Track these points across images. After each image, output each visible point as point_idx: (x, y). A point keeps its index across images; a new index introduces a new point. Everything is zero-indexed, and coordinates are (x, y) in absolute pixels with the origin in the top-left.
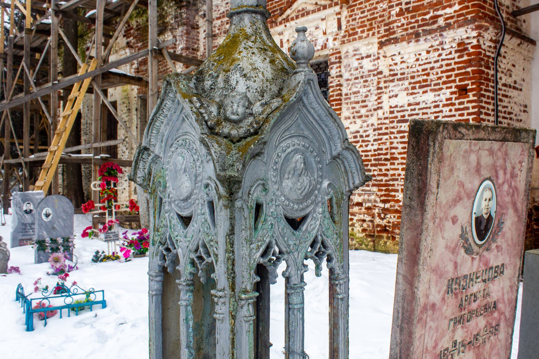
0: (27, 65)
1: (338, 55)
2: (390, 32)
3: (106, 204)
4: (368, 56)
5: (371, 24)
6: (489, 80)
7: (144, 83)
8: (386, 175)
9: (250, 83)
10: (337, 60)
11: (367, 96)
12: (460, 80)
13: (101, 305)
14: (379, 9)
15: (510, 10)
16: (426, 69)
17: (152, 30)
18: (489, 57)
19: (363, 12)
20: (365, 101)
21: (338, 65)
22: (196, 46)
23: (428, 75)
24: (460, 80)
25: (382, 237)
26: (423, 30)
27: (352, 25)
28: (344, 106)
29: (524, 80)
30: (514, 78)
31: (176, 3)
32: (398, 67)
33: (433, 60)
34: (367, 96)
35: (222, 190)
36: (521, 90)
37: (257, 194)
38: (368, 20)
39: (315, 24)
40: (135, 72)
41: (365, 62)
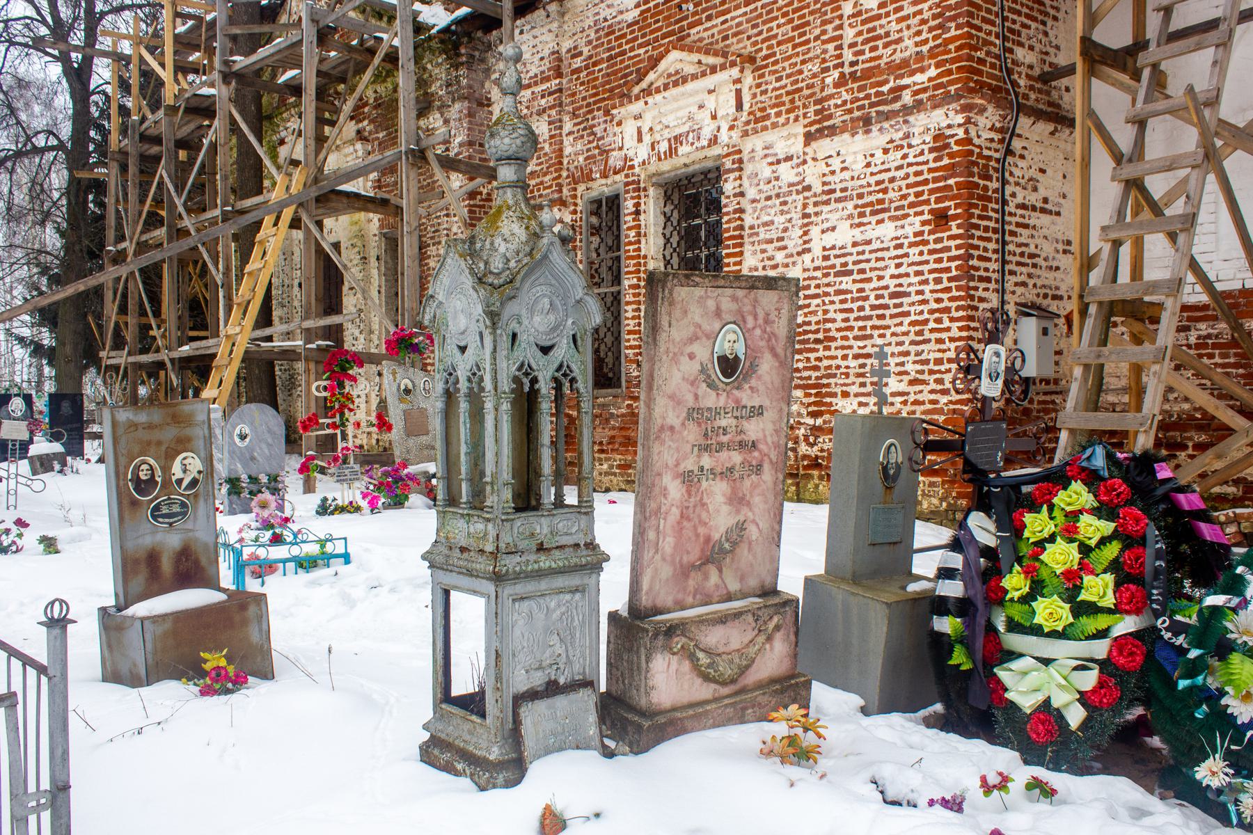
0: (169, 176)
1: (736, 157)
2: (823, 115)
3: (337, 419)
4: (788, 158)
5: (792, 101)
6: (989, 199)
7: (392, 209)
8: (816, 368)
9: (509, 245)
10: (736, 166)
11: (785, 230)
12: (938, 201)
13: (342, 560)
14: (806, 73)
15: (1037, 72)
16: (883, 182)
17: (405, 114)
18: (989, 158)
19: (779, 79)
20: (782, 239)
21: (737, 174)
23: (885, 191)
24: (938, 201)
25: (810, 477)
26: (877, 112)
27: (762, 102)
28: (748, 248)
29: (1064, 197)
30: (1042, 192)
31: (449, 58)
32: (836, 178)
33: (893, 165)
34: (785, 230)
35: (488, 323)
36: (1058, 214)
37: (514, 326)
38: (788, 93)
39: (697, 99)
40: (375, 188)
41: (784, 168)
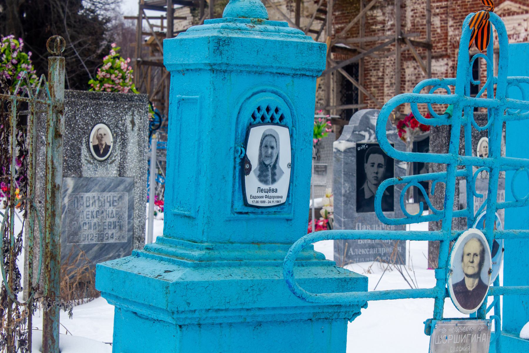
22: (404, 22)
39: (518, 22)
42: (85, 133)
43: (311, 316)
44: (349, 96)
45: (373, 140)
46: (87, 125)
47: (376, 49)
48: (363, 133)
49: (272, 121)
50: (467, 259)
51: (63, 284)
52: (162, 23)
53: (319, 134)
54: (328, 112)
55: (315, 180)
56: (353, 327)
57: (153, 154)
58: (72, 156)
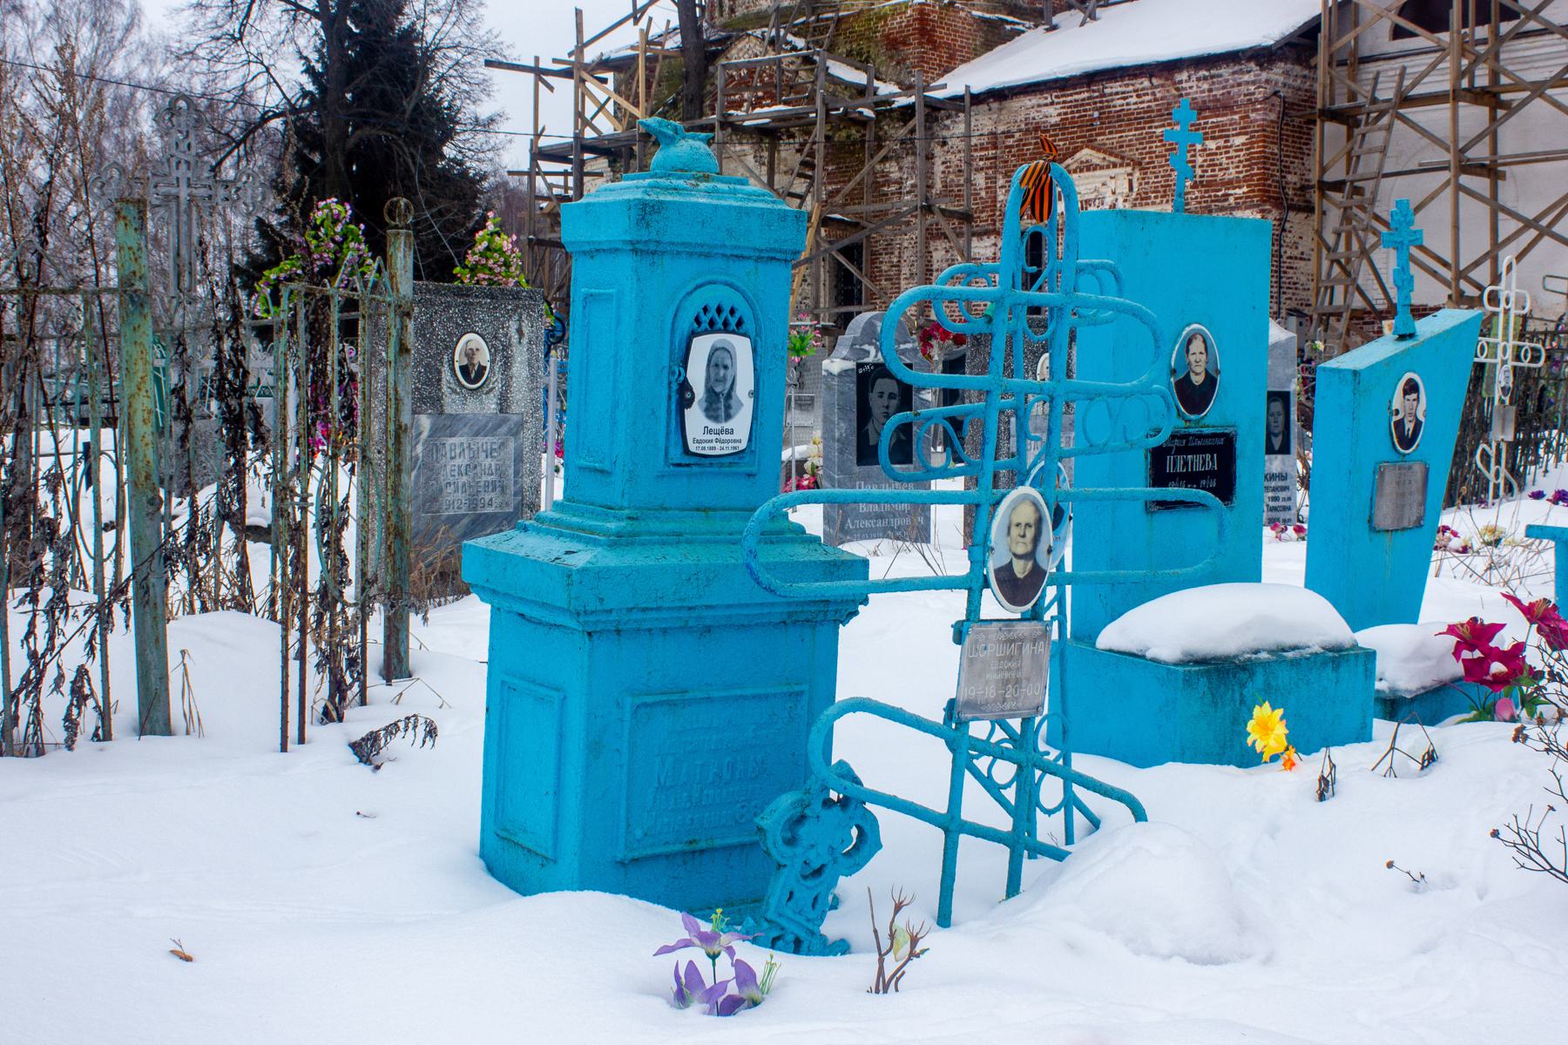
42: (447, 347)
43: (785, 617)
44: (848, 293)
45: (880, 359)
46: (450, 334)
47: (889, 223)
48: (866, 347)
49: (726, 328)
50: (1015, 532)
51: (415, 574)
52: (566, 181)
53: (803, 349)
54: (817, 317)
55: (795, 417)
56: (848, 634)
57: (552, 381)
58: (428, 382)
